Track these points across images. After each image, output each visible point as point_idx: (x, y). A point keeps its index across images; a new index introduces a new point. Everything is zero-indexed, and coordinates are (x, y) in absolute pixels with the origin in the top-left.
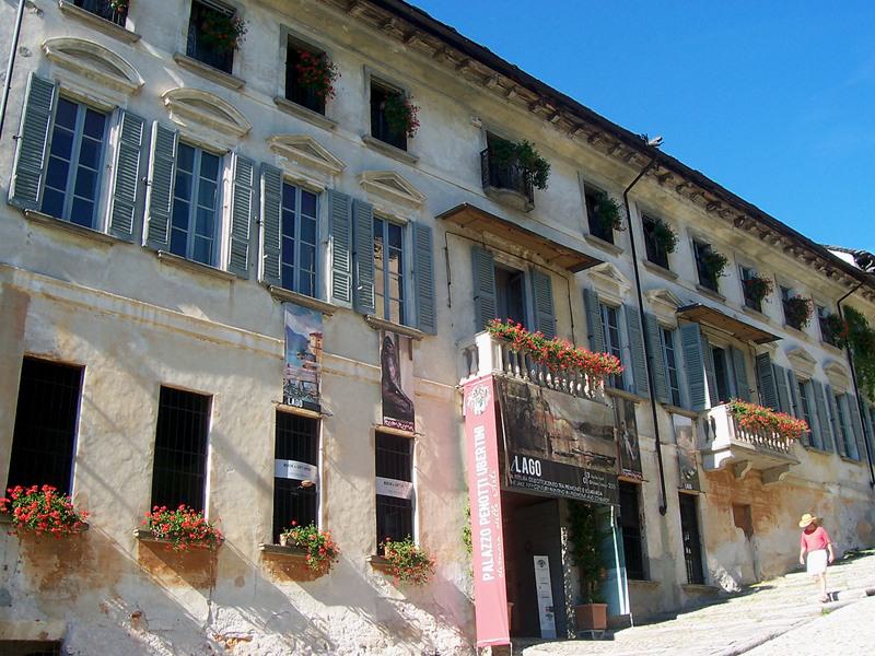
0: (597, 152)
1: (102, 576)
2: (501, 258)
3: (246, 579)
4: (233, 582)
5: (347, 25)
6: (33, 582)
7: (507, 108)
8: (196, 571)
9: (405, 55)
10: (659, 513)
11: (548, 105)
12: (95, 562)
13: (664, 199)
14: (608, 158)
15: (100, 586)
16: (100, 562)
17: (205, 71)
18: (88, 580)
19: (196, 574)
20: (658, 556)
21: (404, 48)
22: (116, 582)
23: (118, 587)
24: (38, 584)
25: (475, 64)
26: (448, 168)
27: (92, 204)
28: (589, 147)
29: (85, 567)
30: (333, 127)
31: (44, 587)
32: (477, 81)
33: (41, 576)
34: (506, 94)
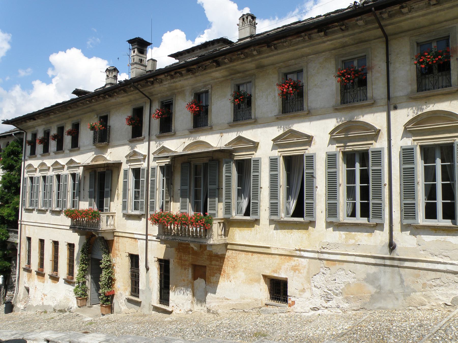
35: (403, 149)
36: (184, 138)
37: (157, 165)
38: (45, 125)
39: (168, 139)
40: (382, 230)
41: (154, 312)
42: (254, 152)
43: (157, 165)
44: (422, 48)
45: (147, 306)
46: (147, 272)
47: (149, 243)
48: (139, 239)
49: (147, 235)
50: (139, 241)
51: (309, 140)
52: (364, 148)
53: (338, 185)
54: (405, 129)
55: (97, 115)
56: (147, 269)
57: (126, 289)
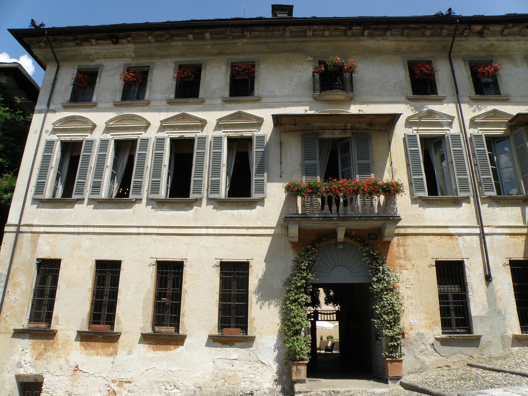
0: (413, 39)
1: (62, 352)
2: (327, 135)
3: (133, 351)
4: (126, 353)
5: (207, 45)
6: (32, 357)
7: (286, 42)
8: (108, 347)
9: (247, 43)
10: (484, 281)
11: (354, 28)
12: (60, 347)
13: (491, 45)
14: (424, 39)
15: (60, 357)
16: (62, 346)
17: (127, 104)
18: (56, 355)
19: (107, 350)
20: (483, 313)
21: (245, 41)
22: (68, 355)
23: (69, 358)
24: (34, 357)
25: (492, 28)
26: (286, 94)
27: (153, 177)
28: (404, 38)
29: (55, 349)
30: (202, 102)
31: (36, 359)
32: (300, 36)
33: (36, 354)
34: (346, 35)
35: (157, 139)
36: (283, 107)
37: (57, 138)
38: (133, 59)
39: (433, 103)
40: (469, 203)
41: (517, 348)
42: (143, 132)
43: (111, 137)
44: (181, 68)
45: (498, 341)
46: (487, 285)
47: (487, 238)
48: (460, 235)
49: (482, 227)
50: (459, 238)
51: (203, 123)
52: (134, 137)
53: (50, 167)
54: (217, 123)
55: (464, 61)
56: (488, 278)
57: (435, 323)
